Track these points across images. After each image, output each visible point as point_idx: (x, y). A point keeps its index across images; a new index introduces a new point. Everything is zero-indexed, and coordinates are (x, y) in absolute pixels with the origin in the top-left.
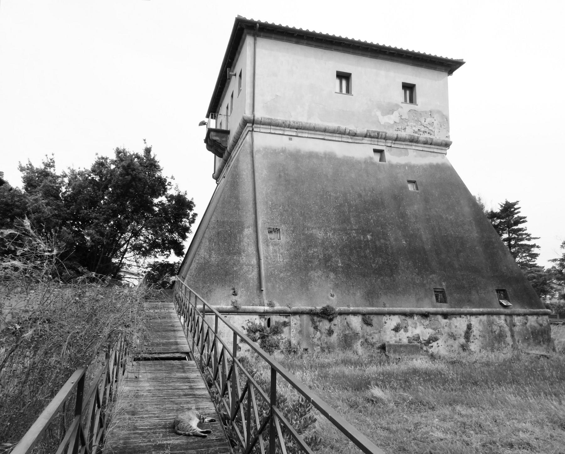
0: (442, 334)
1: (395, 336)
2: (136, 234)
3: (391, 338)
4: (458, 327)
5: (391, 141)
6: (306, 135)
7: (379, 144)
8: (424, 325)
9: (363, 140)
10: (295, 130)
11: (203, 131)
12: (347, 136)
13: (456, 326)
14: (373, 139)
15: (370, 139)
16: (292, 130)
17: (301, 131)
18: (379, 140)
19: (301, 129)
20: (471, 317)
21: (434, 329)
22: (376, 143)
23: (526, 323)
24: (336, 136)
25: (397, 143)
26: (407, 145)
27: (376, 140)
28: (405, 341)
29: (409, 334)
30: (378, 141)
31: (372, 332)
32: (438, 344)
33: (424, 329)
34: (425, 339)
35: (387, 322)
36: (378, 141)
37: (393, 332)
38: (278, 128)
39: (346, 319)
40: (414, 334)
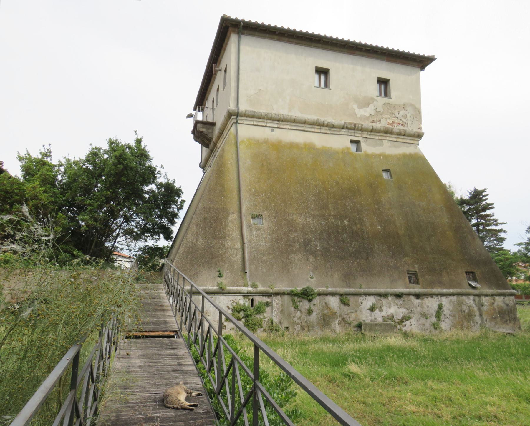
0: (415, 314)
5: (367, 133)
6: (287, 127)
8: (397, 305)
9: (340, 131)
13: (428, 306)
14: (350, 131)
17: (282, 123)
18: (356, 132)
19: (282, 121)
20: (442, 297)
22: (353, 134)
23: (493, 303)
28: (380, 320)
29: (384, 313)
30: (354, 133)
31: (349, 311)
32: (410, 322)
35: (363, 302)
37: (369, 311)
38: (261, 120)
39: (324, 299)
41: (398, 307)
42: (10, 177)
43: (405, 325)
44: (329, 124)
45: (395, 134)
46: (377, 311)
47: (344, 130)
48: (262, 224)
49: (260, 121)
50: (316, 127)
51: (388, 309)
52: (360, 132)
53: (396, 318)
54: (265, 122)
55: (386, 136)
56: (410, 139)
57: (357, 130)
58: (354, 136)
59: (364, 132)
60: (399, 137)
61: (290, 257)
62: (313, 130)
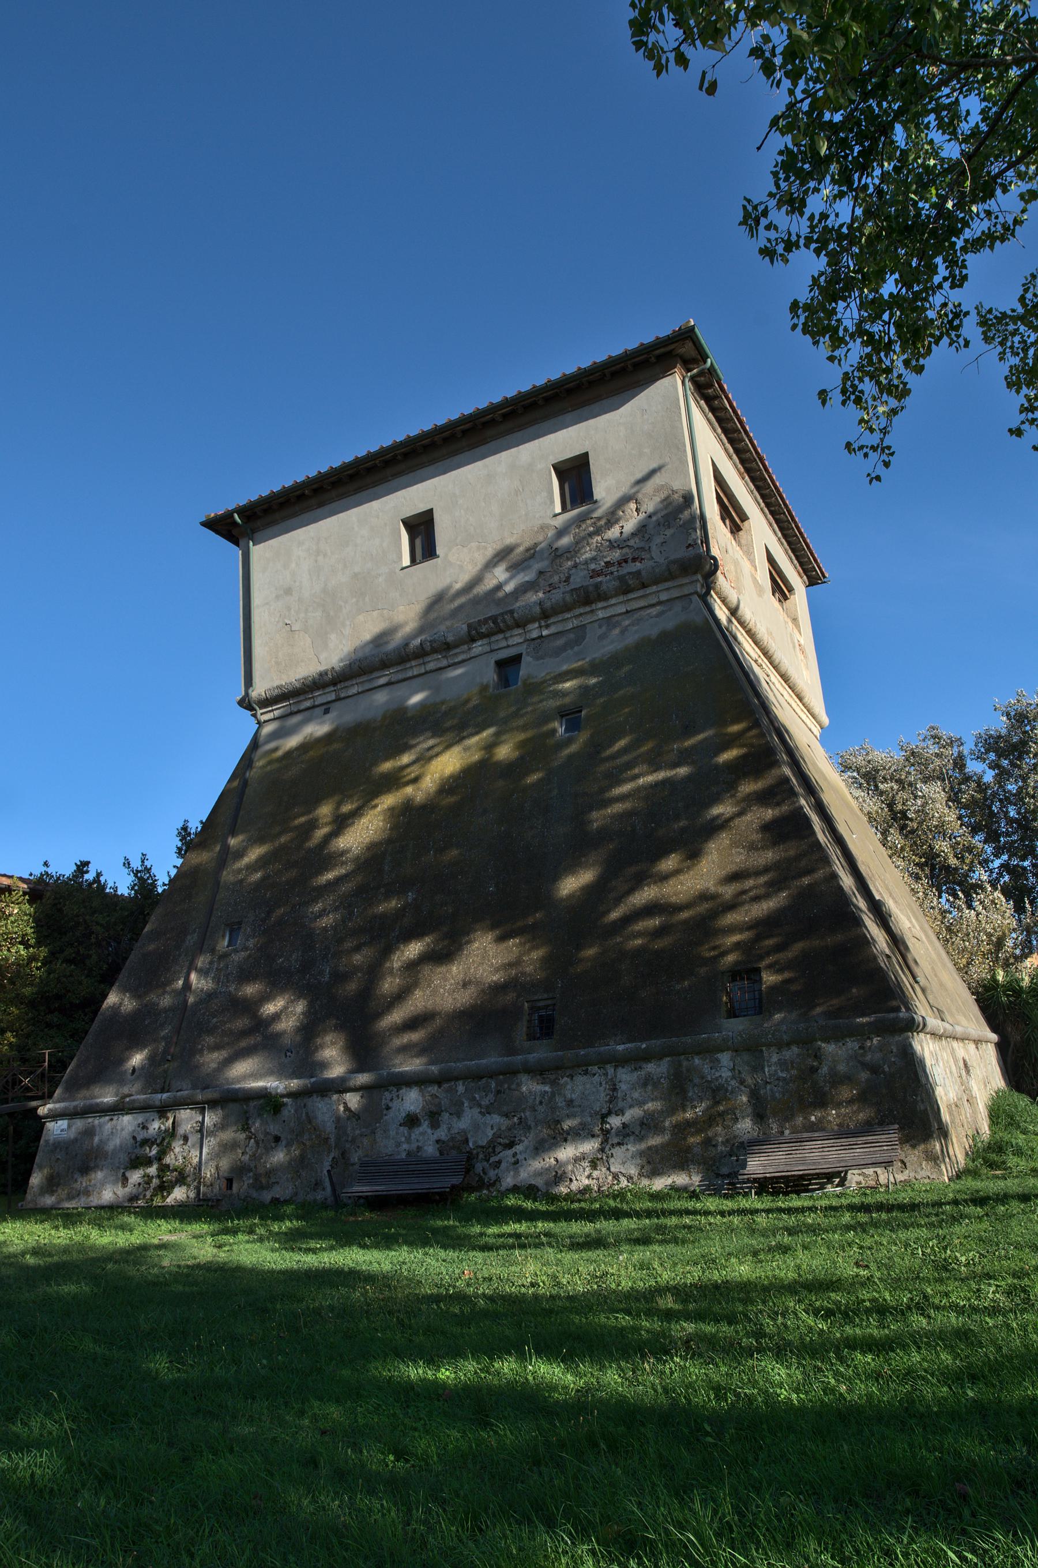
0: (530, 1128)
1: (408, 1140)
2: (607, 1394)
3: (398, 1144)
4: (576, 1103)
5: (536, 625)
6: (354, 690)
7: (511, 642)
8: (480, 1106)
9: (469, 649)
10: (332, 689)
11: (704, 92)
12: (435, 656)
13: (571, 1101)
14: (493, 639)
15: (485, 641)
16: (327, 690)
17: (343, 685)
18: (508, 634)
19: (340, 682)
20: (620, 1070)
21: (506, 1116)
22: (504, 644)
23: (814, 1070)
24: (411, 667)
25: (554, 623)
26: (581, 614)
27: (501, 636)
28: (430, 1150)
29: (442, 1133)
30: (506, 639)
31: (357, 1132)
32: (515, 1155)
33: (480, 1116)
34: (480, 1143)
35: (390, 1105)
36: (506, 639)
37: (404, 1130)
38: (302, 697)
39: (305, 1106)
40: (455, 1131)
41: (480, 1112)
42: (566, 1140)
43: (500, 1162)
44: (435, 645)
45: (616, 595)
46: (425, 1126)
47: (480, 643)
48: (732, 1014)
49: (301, 701)
50: (413, 663)
51: (455, 1119)
52: (520, 631)
53: (475, 1142)
54: (310, 698)
55: (592, 611)
56: (668, 589)
57: (509, 628)
58: (508, 646)
59: (530, 627)
60: (631, 596)
61: (562, 1081)
62: (410, 674)
